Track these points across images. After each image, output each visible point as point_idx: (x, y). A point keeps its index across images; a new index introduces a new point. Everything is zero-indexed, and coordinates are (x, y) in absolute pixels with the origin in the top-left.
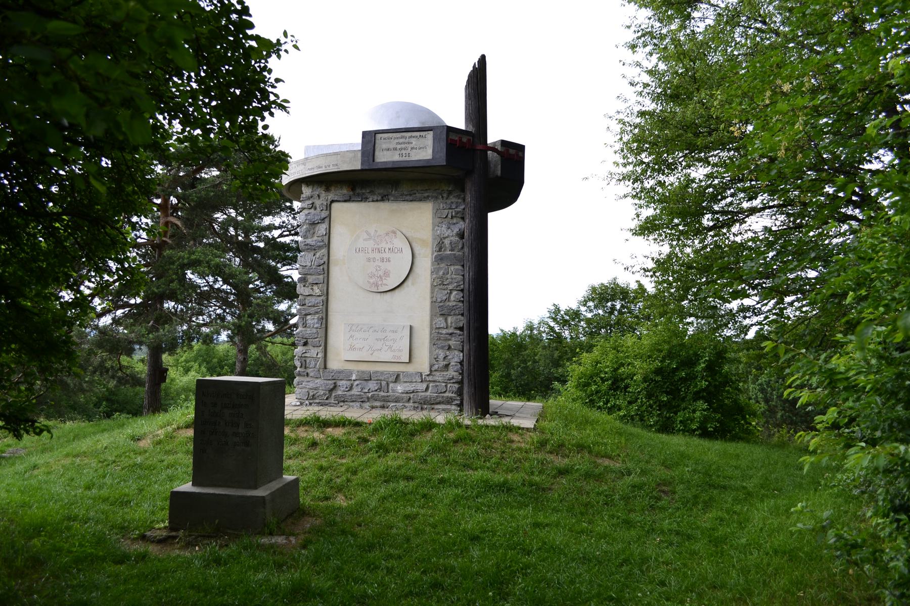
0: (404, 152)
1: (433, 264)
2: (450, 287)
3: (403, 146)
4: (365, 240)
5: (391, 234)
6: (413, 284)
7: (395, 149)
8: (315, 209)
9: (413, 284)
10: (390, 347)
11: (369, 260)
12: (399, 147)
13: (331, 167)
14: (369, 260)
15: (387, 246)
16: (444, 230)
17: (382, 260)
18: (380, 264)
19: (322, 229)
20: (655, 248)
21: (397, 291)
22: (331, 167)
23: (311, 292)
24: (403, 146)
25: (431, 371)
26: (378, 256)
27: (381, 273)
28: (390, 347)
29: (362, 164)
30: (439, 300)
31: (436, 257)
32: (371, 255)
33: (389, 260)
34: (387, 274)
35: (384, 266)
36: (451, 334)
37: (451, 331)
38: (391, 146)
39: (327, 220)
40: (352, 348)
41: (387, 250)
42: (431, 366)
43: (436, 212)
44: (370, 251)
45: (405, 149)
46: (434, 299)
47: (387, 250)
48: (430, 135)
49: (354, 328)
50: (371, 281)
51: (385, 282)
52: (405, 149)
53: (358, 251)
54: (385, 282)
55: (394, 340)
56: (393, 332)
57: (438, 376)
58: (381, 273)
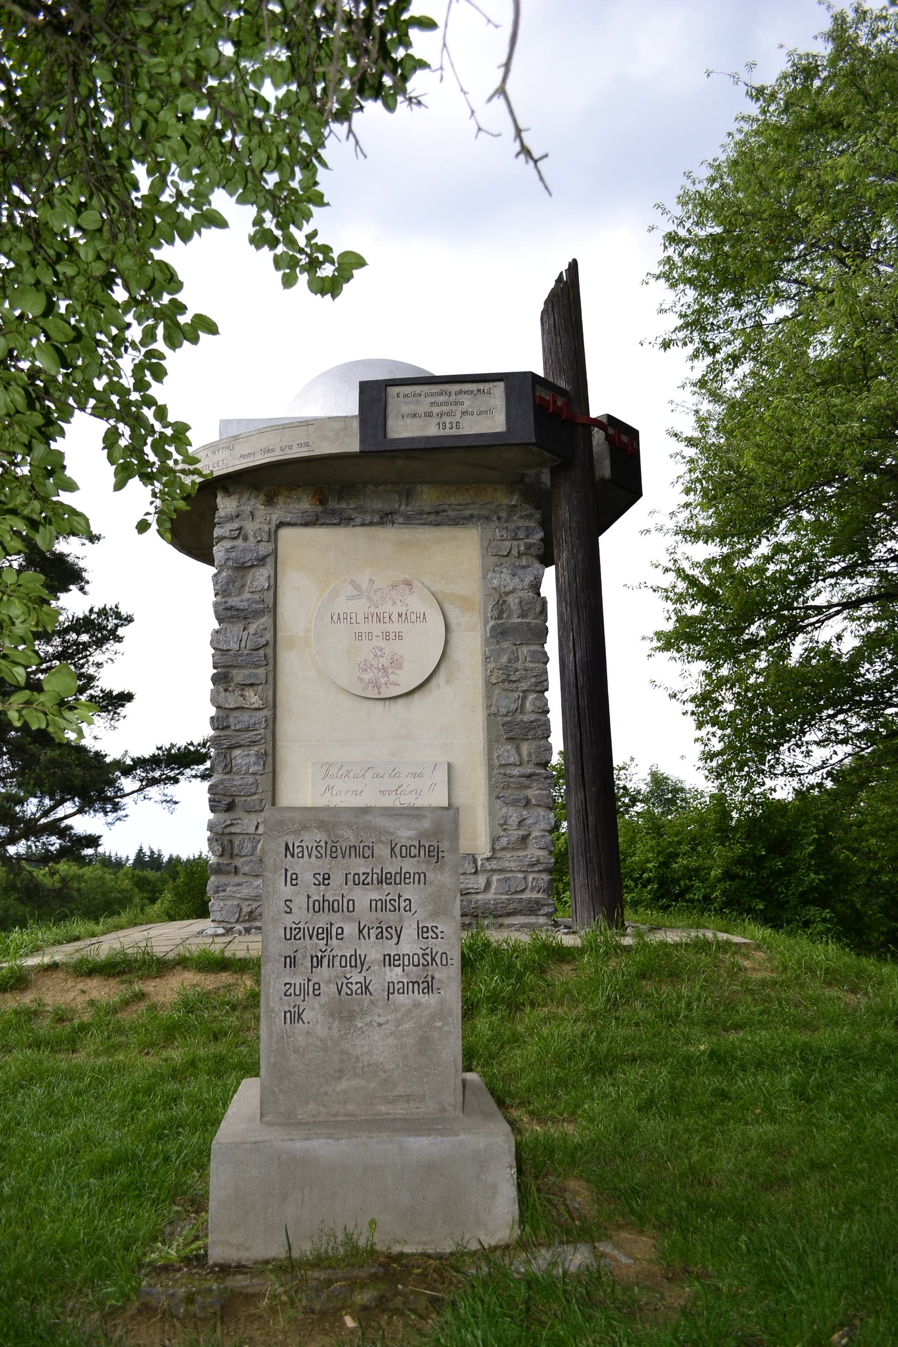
0: (447, 420)
1: (487, 643)
2: (524, 686)
3: (445, 409)
7: (429, 415)
8: (246, 539)
9: (448, 682)
12: (436, 410)
14: (359, 636)
15: (396, 610)
17: (387, 636)
18: (382, 644)
19: (260, 577)
22: (278, 452)
23: (241, 702)
24: (445, 409)
25: (493, 850)
26: (377, 628)
27: (384, 661)
29: (362, 442)
30: (503, 711)
31: (493, 629)
32: (363, 628)
33: (399, 636)
34: (396, 663)
36: (529, 776)
37: (529, 770)
38: (421, 410)
39: (270, 561)
41: (395, 617)
43: (486, 548)
46: (494, 709)
47: (395, 617)
48: (501, 385)
49: (333, 771)
50: (366, 677)
51: (392, 678)
52: (448, 414)
53: (337, 619)
54: (392, 678)
56: (414, 775)
57: (509, 860)
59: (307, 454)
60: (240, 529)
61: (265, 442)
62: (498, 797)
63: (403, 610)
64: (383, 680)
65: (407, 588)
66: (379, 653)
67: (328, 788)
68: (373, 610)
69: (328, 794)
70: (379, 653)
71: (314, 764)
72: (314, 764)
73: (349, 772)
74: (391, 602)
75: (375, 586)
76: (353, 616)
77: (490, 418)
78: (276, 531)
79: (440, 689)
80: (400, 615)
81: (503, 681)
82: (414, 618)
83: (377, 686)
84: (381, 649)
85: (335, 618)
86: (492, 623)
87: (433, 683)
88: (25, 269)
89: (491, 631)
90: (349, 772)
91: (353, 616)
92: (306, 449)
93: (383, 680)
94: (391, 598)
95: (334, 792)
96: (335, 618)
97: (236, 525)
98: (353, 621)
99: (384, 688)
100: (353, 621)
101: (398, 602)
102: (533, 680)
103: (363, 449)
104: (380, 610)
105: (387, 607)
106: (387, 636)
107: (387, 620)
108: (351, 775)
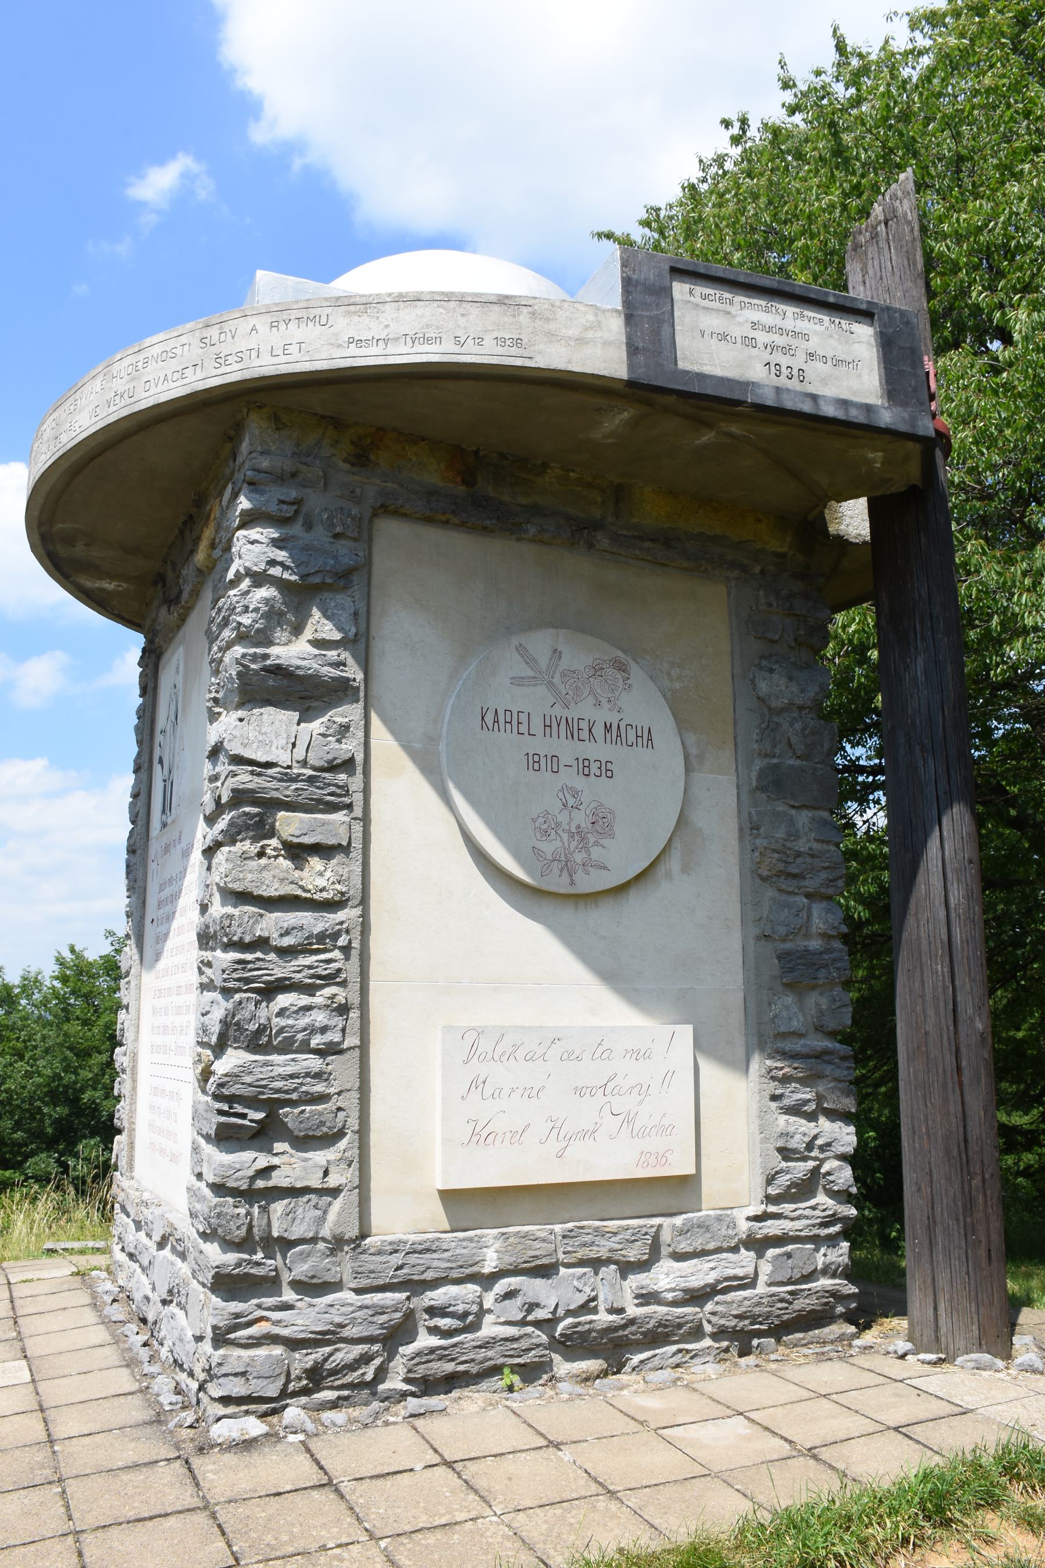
4: (518, 681)
5: (611, 672)
6: (685, 869)
8: (308, 526)
9: (685, 869)
10: (629, 1120)
11: (534, 762)
12: (762, 337)
13: (489, 343)
14: (534, 762)
15: (603, 716)
16: (776, 686)
17: (584, 767)
18: (579, 782)
20: (309, 859)
21: (634, 899)
22: (489, 343)
24: (781, 341)
26: (567, 750)
27: (581, 818)
28: (629, 1120)
32: (541, 745)
33: (607, 771)
34: (602, 823)
35: (594, 791)
36: (820, 1056)
38: (737, 332)
40: (480, 1135)
41: (599, 731)
42: (770, 1180)
44: (537, 726)
45: (786, 350)
47: (599, 731)
50: (548, 848)
51: (596, 853)
52: (786, 350)
53: (493, 720)
54: (596, 853)
55: (642, 1090)
56: (639, 1055)
57: (800, 1217)
58: (581, 818)
59: (518, 362)
60: (298, 502)
61: (410, 319)
62: (774, 1098)
63: (613, 718)
64: (579, 857)
65: (619, 676)
66: (571, 801)
67: (477, 1084)
68: (559, 711)
69: (475, 1094)
70: (571, 801)
71: (448, 1029)
72: (448, 1029)
73: (516, 1047)
74: (591, 700)
75: (564, 664)
76: (523, 718)
77: (621, 386)
78: (371, 521)
79: (674, 889)
80: (608, 728)
81: (780, 874)
82: (632, 738)
83: (568, 868)
84: (575, 794)
85: (489, 718)
86: (758, 764)
87: (661, 870)
88: (203, 953)
89: (759, 777)
90: (516, 1047)
91: (523, 718)
92: (514, 351)
93: (579, 857)
94: (592, 692)
95: (488, 1092)
96: (489, 718)
97: (293, 494)
98: (523, 728)
99: (579, 875)
100: (523, 728)
101: (604, 701)
102: (824, 875)
103: (644, 376)
104: (573, 714)
105: (584, 710)
106: (584, 767)
107: (585, 734)
108: (520, 1054)
